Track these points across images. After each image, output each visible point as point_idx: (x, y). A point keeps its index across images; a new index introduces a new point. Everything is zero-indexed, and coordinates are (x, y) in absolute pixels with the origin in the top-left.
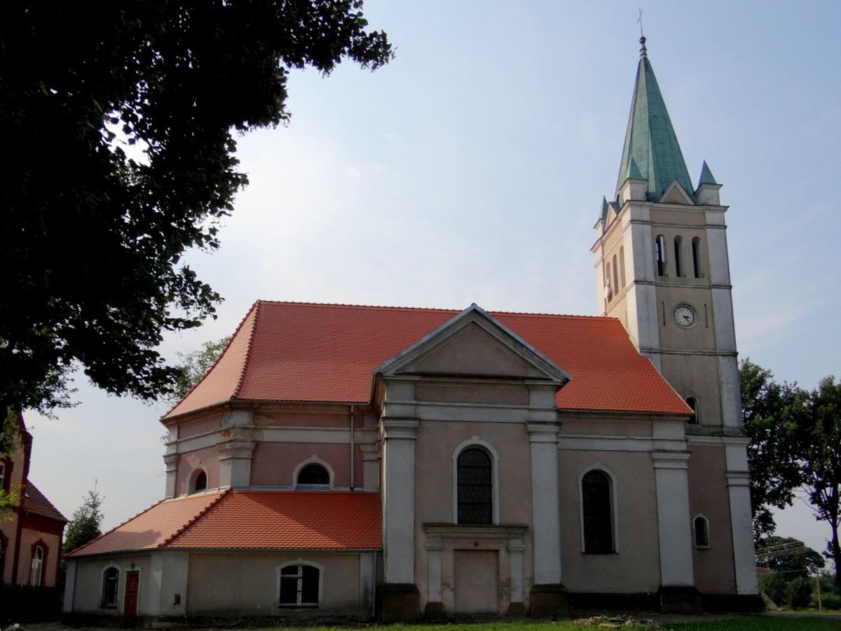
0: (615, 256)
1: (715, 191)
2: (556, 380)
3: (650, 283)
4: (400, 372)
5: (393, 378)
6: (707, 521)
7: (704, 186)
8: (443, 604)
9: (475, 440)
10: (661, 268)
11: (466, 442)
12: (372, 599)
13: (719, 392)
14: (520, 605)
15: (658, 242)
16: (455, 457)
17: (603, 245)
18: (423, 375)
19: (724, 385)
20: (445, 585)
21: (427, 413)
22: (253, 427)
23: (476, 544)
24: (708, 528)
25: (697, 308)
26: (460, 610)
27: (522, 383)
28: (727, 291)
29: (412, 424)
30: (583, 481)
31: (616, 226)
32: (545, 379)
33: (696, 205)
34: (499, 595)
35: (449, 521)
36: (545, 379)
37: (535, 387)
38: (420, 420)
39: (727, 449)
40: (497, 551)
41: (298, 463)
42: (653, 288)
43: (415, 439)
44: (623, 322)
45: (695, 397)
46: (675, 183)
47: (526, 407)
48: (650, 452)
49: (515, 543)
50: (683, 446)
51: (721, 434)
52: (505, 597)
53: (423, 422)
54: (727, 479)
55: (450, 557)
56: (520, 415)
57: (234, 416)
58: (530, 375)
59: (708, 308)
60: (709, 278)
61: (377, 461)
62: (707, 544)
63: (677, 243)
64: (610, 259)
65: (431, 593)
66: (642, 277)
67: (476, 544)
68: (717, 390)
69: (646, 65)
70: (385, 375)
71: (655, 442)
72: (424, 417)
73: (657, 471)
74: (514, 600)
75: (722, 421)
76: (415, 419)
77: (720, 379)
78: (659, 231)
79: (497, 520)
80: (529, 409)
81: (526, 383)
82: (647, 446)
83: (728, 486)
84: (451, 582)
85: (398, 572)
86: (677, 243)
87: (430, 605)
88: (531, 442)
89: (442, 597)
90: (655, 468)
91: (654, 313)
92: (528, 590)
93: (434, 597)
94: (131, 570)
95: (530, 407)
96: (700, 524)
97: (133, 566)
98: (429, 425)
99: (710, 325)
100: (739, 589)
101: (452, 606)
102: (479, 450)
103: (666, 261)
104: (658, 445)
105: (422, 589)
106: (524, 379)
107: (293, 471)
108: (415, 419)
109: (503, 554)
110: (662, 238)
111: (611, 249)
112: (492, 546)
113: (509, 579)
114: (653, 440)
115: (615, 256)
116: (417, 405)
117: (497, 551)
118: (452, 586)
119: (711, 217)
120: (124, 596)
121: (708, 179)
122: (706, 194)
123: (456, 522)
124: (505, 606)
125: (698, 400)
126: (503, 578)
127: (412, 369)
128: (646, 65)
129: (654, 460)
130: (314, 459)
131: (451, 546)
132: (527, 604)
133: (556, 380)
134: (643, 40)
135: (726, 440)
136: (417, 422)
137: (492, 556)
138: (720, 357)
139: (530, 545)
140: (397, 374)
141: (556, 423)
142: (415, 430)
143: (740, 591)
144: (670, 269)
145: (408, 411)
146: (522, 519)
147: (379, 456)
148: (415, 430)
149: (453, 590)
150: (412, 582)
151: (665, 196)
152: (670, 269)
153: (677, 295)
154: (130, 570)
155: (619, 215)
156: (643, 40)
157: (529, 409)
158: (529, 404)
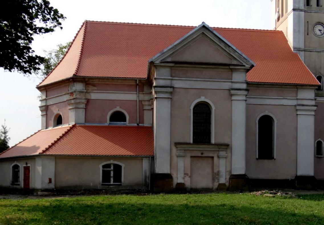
2: (247, 66)
3: (301, 10)
4: (163, 61)
5: (160, 65)
9: (203, 99)
14: (224, 185)
20: (186, 174)
21: (177, 84)
23: (202, 154)
26: (194, 186)
34: (213, 179)
35: (188, 141)
38: (173, 88)
40: (213, 158)
41: (109, 111)
42: (303, 13)
43: (171, 98)
47: (230, 81)
48: (295, 106)
49: (222, 153)
50: (313, 103)
52: (216, 181)
55: (188, 160)
56: (227, 85)
57: (75, 85)
58: (233, 63)
66: (297, 6)
67: (202, 154)
71: (298, 100)
76: (171, 87)
79: (213, 141)
81: (230, 68)
82: (294, 102)
87: (178, 184)
90: (297, 115)
91: (302, 28)
92: (228, 177)
93: (180, 180)
95: (232, 81)
97: (27, 164)
98: (178, 90)
104: (300, 102)
105: (174, 176)
106: (229, 65)
107: (107, 114)
108: (171, 87)
109: (216, 159)
112: (211, 155)
114: (297, 99)
117: (213, 158)
118: (189, 175)
123: (192, 142)
124: (216, 185)
125: (323, 77)
126: (216, 171)
127: (169, 60)
129: (297, 110)
132: (227, 184)
136: (172, 89)
137: (210, 160)
139: (230, 154)
141: (247, 90)
142: (171, 93)
145: (167, 83)
146: (226, 141)
147: (152, 107)
149: (190, 177)
150: (169, 173)
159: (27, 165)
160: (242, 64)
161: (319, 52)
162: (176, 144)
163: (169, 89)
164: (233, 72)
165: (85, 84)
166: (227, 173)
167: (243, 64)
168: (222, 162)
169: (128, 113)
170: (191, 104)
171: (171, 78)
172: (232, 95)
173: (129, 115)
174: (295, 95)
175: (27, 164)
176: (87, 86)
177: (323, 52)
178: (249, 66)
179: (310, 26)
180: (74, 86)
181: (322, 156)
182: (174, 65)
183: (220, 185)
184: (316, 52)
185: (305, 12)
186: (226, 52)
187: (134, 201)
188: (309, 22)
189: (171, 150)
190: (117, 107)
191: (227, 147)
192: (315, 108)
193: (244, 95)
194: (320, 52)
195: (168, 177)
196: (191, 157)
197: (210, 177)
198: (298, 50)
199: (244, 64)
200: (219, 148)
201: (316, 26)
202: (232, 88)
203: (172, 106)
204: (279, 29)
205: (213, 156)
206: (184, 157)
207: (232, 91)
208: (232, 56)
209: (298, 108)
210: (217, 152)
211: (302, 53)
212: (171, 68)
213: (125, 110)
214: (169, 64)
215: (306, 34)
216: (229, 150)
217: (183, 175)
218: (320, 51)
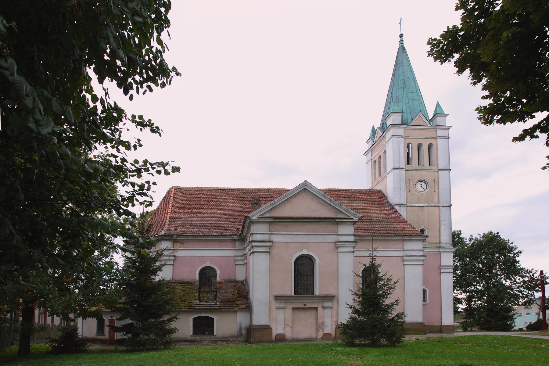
0: (380, 157)
1: (444, 118)
2: (354, 218)
3: (402, 169)
4: (260, 217)
5: (257, 220)
6: (428, 291)
7: (437, 115)
8: (285, 334)
9: (305, 252)
10: (408, 161)
11: (297, 254)
12: (244, 332)
13: (440, 225)
14: (330, 334)
15: (408, 147)
16: (293, 261)
17: (372, 151)
18: (275, 218)
19: (442, 222)
20: (286, 325)
21: (275, 238)
22: (173, 248)
23: (305, 305)
24: (428, 294)
25: (429, 182)
26: (295, 336)
27: (334, 221)
28: (448, 172)
29: (270, 244)
30: (362, 272)
31: (382, 140)
32: (348, 218)
33: (432, 126)
34: (317, 329)
35: (289, 294)
36: (348, 218)
37: (342, 223)
38: (272, 242)
39: (441, 254)
40: (316, 309)
41: (199, 266)
42: (403, 172)
43: (270, 252)
44: (384, 192)
45: (425, 228)
46: (420, 114)
47: (336, 233)
48: (402, 257)
49: (327, 304)
50: (421, 253)
51: (440, 247)
52: (321, 330)
53: (274, 243)
54: (440, 269)
55: (289, 311)
56: (333, 238)
57: (163, 244)
58: (339, 216)
59: (436, 181)
60: (438, 166)
61: (244, 265)
62: (427, 302)
63: (419, 146)
64: (377, 158)
65: (278, 329)
66: (397, 166)
67: (305, 305)
68: (438, 225)
69: (402, 50)
70: (251, 218)
71: (405, 251)
72: (275, 240)
73: (405, 266)
74: (325, 332)
75: (440, 241)
76: (270, 241)
77: (440, 219)
78: (409, 141)
79: (317, 292)
80: (338, 235)
81: (336, 221)
82: (401, 254)
83: (441, 273)
84: (290, 324)
85: (259, 319)
86: (419, 146)
87: (277, 335)
88: (338, 252)
89: (285, 331)
90: (404, 265)
91: (403, 185)
92: (334, 327)
93: (280, 331)
94: (111, 319)
95: (338, 234)
96: (424, 291)
97: (112, 317)
98: (277, 244)
99: (437, 191)
100: (442, 323)
101: (291, 335)
102: (306, 257)
103: (412, 157)
104: (407, 253)
105: (273, 327)
106: (335, 219)
107: (196, 270)
108: (270, 241)
109: (320, 310)
110: (410, 145)
111: (378, 152)
112: (314, 306)
113: (323, 322)
114: (404, 250)
115: (380, 157)
116: (271, 234)
117: (316, 309)
118: (290, 325)
119: (440, 133)
120: (108, 331)
121: (439, 112)
122: (439, 120)
123: (293, 294)
124: (320, 335)
125: (426, 230)
126: (320, 321)
127: (268, 215)
128: (402, 50)
129: (403, 261)
130: (208, 264)
131: (290, 306)
132: (333, 334)
133: (354, 218)
134: (401, 36)
135: (441, 250)
136: (271, 243)
137: (314, 312)
138: (441, 207)
139: (336, 305)
140: (258, 218)
141: (355, 242)
142: (270, 247)
143: (443, 324)
144: (415, 161)
145: (266, 237)
146: (332, 292)
147: (245, 262)
148: (270, 247)
149: (291, 327)
150: (268, 324)
151: (413, 121)
152: (415, 161)
153: (418, 175)
154: (110, 318)
155: (384, 133)
156: (401, 36)
157: (338, 235)
158: (338, 232)
159: (112, 318)
160: (349, 217)
161: (421, 207)
162: (278, 298)
163: (268, 243)
164: (339, 225)
165: (172, 242)
166: (334, 323)
167: (350, 217)
168: (328, 312)
169: (219, 268)
170: (292, 258)
171: (270, 233)
172: (338, 247)
173: (220, 270)
174: (401, 246)
175: (112, 317)
176: (175, 244)
177: (425, 206)
178: (358, 219)
179: (411, 183)
180: (162, 244)
181: (426, 303)
182: (273, 220)
183: (325, 335)
184: (419, 206)
185: (406, 170)
186: (331, 206)
187: (44, 133)
188: (410, 180)
189: (269, 302)
190: (207, 262)
191: (331, 298)
192: (423, 258)
193: (352, 247)
194: (423, 207)
195: (267, 328)
196: (293, 308)
197: (314, 328)
198: (400, 205)
199: (351, 217)
200: (324, 299)
201: (418, 183)
202: (339, 241)
203: (271, 259)
204: (376, 188)
205: (317, 307)
206: (285, 308)
207: (338, 243)
208: (338, 209)
209: (405, 258)
210: (322, 303)
211: (403, 209)
212: (270, 223)
213: (216, 266)
214: (270, 219)
215: (408, 190)
216: (335, 301)
217: (283, 326)
218: (423, 206)
